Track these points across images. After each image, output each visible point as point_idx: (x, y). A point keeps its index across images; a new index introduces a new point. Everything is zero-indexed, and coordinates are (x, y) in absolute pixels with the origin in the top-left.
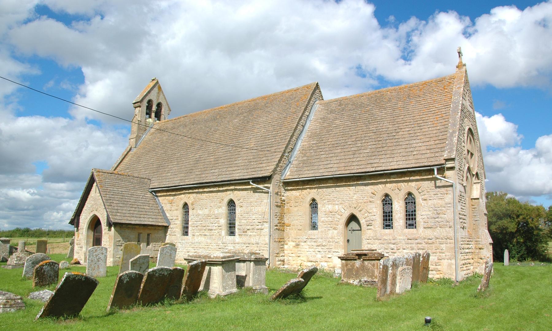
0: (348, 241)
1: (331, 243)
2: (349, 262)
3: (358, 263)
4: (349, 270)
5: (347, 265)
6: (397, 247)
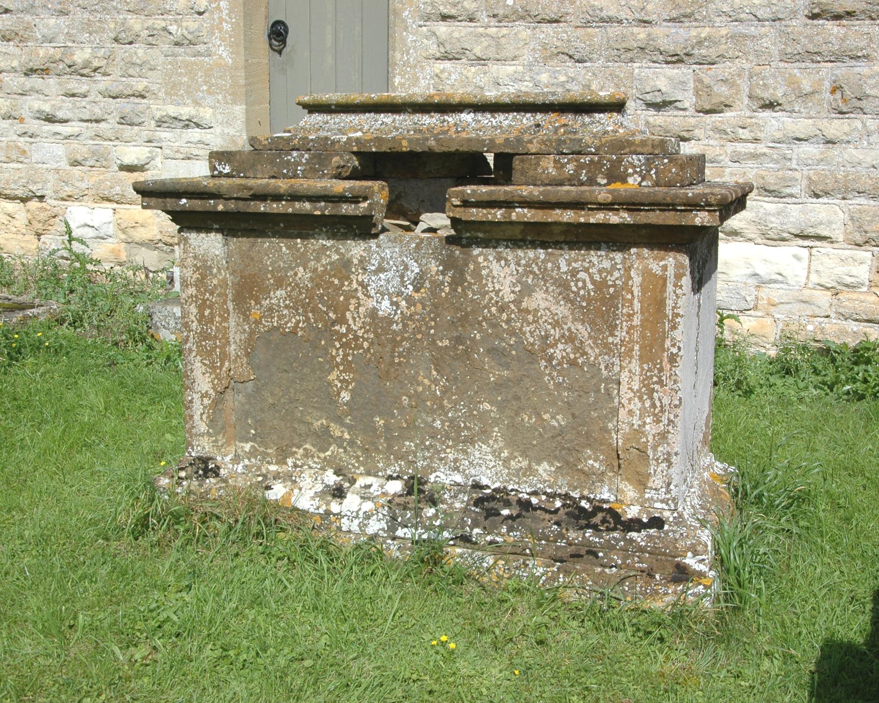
0: (278, 33)
1: (140, 51)
2: (275, 251)
3: (389, 271)
4: (269, 346)
5: (248, 289)
6: (702, 89)
